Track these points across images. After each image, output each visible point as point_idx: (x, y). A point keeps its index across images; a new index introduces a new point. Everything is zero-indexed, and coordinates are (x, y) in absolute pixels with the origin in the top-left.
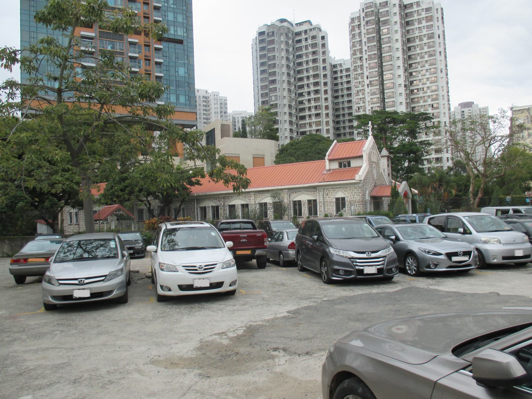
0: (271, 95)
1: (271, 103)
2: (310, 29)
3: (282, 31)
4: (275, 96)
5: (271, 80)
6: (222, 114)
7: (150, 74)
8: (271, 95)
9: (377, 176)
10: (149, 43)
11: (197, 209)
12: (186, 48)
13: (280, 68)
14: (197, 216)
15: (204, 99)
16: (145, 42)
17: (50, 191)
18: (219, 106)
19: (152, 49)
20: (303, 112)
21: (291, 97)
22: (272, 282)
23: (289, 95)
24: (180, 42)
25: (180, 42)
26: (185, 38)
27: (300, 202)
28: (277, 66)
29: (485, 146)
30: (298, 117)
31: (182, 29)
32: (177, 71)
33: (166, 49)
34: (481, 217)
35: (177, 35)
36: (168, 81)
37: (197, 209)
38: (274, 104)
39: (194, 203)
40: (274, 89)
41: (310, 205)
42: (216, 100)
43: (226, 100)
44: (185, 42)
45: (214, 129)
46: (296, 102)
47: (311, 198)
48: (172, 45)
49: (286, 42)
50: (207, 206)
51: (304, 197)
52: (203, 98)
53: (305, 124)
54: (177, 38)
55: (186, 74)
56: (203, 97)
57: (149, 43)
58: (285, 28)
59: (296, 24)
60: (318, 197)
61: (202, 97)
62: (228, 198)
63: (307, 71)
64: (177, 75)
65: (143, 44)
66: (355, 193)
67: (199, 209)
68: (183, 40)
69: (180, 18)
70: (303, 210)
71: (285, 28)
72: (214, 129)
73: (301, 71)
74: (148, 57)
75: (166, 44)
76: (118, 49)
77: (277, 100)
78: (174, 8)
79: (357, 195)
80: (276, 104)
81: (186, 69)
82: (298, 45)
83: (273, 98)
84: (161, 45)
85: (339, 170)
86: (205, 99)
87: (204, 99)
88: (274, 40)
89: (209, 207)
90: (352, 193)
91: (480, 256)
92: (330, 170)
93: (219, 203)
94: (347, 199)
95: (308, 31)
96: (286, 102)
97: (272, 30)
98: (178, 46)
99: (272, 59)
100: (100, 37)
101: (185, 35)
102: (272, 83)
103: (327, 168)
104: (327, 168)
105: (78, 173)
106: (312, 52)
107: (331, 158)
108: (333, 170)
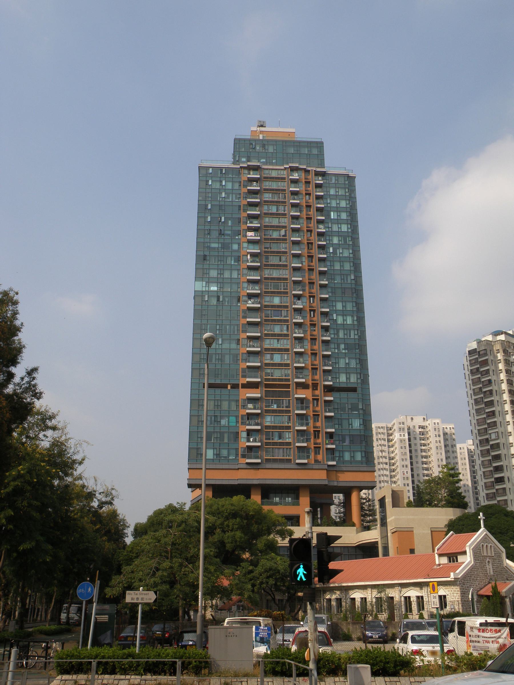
0: (490, 432)
1: (491, 443)
6: (448, 448)
7: (319, 415)
8: (490, 432)
9: (493, 572)
14: (246, 619)
15: (420, 430)
18: (442, 439)
24: (354, 390)
25: (354, 390)
26: (360, 385)
27: (409, 597)
28: (494, 392)
29: (164, 627)
31: (356, 375)
32: (350, 423)
35: (350, 383)
36: (340, 437)
37: (323, 600)
38: (495, 444)
40: (493, 425)
42: (437, 430)
44: (359, 390)
45: (385, 496)
47: (420, 594)
48: (344, 395)
51: (413, 593)
52: (419, 428)
54: (349, 386)
55: (361, 426)
56: (420, 427)
60: (423, 593)
61: (417, 427)
64: (350, 428)
66: (454, 591)
70: (425, 604)
72: (385, 496)
75: (337, 394)
76: (284, 407)
78: (345, 353)
79: (456, 594)
80: (498, 444)
81: (361, 420)
83: (493, 436)
85: (448, 565)
86: (422, 430)
87: (420, 430)
88: (487, 360)
90: (451, 591)
92: (439, 565)
94: (448, 597)
98: (351, 394)
103: (437, 563)
104: (437, 563)
107: (440, 552)
108: (442, 564)
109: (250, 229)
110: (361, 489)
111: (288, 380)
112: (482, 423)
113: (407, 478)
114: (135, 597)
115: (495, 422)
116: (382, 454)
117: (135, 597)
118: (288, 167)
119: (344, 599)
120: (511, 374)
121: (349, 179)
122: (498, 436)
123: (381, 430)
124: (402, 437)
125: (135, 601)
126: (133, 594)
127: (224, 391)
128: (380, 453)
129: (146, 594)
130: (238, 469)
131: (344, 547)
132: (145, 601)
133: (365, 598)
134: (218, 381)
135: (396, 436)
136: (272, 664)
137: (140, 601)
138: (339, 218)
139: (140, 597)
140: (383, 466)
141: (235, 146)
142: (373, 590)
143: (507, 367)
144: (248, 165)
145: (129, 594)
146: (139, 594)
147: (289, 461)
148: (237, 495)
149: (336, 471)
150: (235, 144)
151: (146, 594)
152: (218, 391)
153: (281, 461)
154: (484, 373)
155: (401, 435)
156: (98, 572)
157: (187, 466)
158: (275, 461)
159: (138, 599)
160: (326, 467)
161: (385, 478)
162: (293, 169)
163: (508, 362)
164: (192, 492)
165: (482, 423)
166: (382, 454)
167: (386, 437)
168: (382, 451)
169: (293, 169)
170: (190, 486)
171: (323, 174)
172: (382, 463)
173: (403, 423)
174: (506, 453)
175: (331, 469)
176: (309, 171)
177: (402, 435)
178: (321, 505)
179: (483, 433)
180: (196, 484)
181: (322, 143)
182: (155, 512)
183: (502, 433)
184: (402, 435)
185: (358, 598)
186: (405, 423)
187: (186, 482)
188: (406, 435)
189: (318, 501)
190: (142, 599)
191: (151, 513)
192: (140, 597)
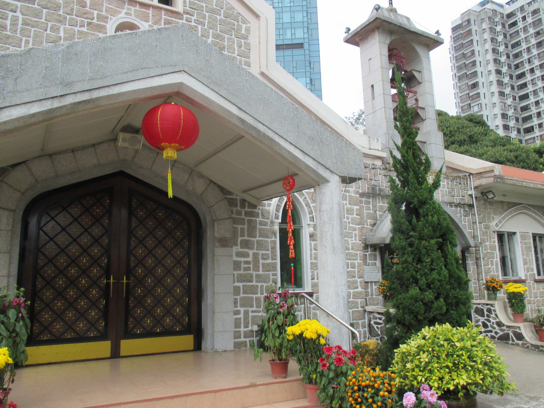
2: (528, 3)
3: (483, 16)
4: (478, 105)
5: (472, 84)
13: (485, 67)
20: (529, 121)
21: (505, 104)
23: (500, 101)
24: (300, 46)
26: (306, 40)
30: (522, 131)
34: (467, 13)
40: (476, 96)
41: (296, 226)
43: (419, 129)
44: (306, 46)
46: (515, 110)
49: (490, 28)
53: (534, 138)
54: (295, 42)
58: (488, 11)
59: (506, 4)
63: (529, 62)
64: (293, 37)
69: (299, 17)
71: (488, 11)
73: (520, 65)
77: (481, 110)
82: (514, 30)
91: (428, 310)
95: (526, 7)
96: (498, 111)
97: (467, 18)
99: (470, 56)
101: (306, 36)
102: (472, 88)
106: (535, 33)
109: (316, 376)
112: (466, 100)
115: (479, 93)
120: (507, 119)
122: (481, 107)
136: (297, 295)
138: (293, 37)
143: (500, 88)
154: (474, 97)
156: (111, 296)
163: (501, 84)
165: (466, 100)
174: (488, 114)
179: (466, 109)
183: (486, 105)
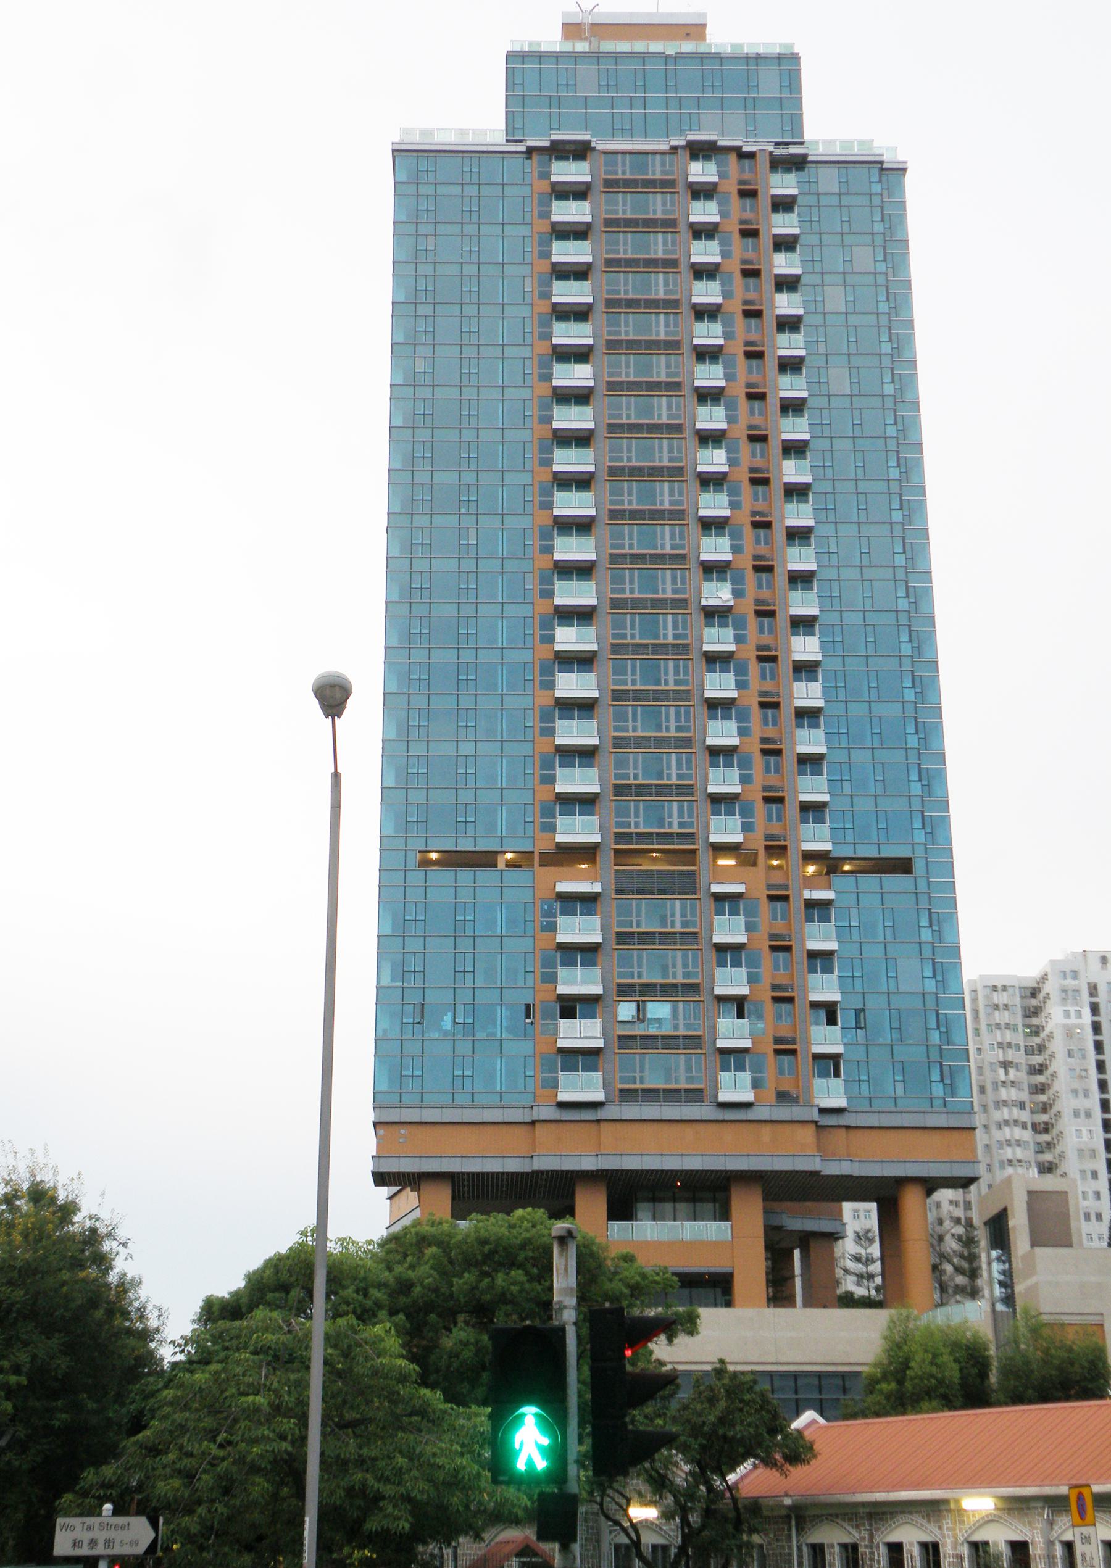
10: (786, 888)
11: (799, 1549)
12: (922, 885)
16: (770, 887)
17: (528, 1281)
19: (796, 906)
22: (145, 1486)
24: (903, 866)
25: (903, 866)
33: (851, 900)
39: (790, 1530)
44: (919, 866)
45: (1005, 1210)
50: (826, 1542)
57: (786, 888)
60: (1066, 1529)
62: (881, 1519)
65: (762, 893)
67: (805, 1549)
68: (910, 859)
72: (1005, 1210)
74: (769, 605)
84: (829, 887)
89: (832, 1546)
93: (857, 1535)
98: (894, 882)
100: (619, 891)
105: (618, 1277)
110: (930, 1185)
111: (690, 837)
113: (1093, 1153)
114: (86, 1536)
116: (1007, 1073)
117: (86, 1536)
118: (683, 143)
119: (866, 1546)
121: (884, 178)
123: (1000, 998)
124: (1073, 1020)
125: (85, 1551)
126: (79, 1528)
127: (485, 875)
128: (1001, 1071)
129: (123, 1527)
130: (533, 1123)
131: (783, 1375)
132: (117, 1550)
133: (936, 1546)
134: (466, 845)
135: (1055, 1017)
137: (100, 1550)
139: (101, 1536)
140: (1010, 1113)
141: (510, 121)
142: (1096, 1514)
144: (552, 142)
145: (65, 1527)
146: (97, 1527)
147: (695, 1096)
148: (524, 1208)
149: (847, 1127)
150: (510, 73)
151: (123, 1527)
152: (465, 875)
153: (672, 1095)
155: (1067, 1014)
157: (370, 1116)
158: (651, 1095)
159: (93, 1543)
160: (816, 1116)
161: (1019, 1153)
162: (700, 150)
164: (391, 1198)
166: (1007, 1073)
167: (1019, 1020)
168: (1006, 1065)
169: (700, 150)
170: (381, 1179)
171: (798, 163)
172: (1005, 1103)
173: (1075, 974)
175: (832, 1120)
176: (751, 155)
177: (1072, 1014)
178: (806, 1240)
180: (399, 1173)
181: (795, 58)
182: (268, 1263)
184: (1072, 1014)
185: (911, 1544)
186: (1082, 974)
187: (369, 1166)
188: (1087, 1012)
189: (795, 1224)
190: (108, 1543)
191: (255, 1263)
192: (101, 1536)
